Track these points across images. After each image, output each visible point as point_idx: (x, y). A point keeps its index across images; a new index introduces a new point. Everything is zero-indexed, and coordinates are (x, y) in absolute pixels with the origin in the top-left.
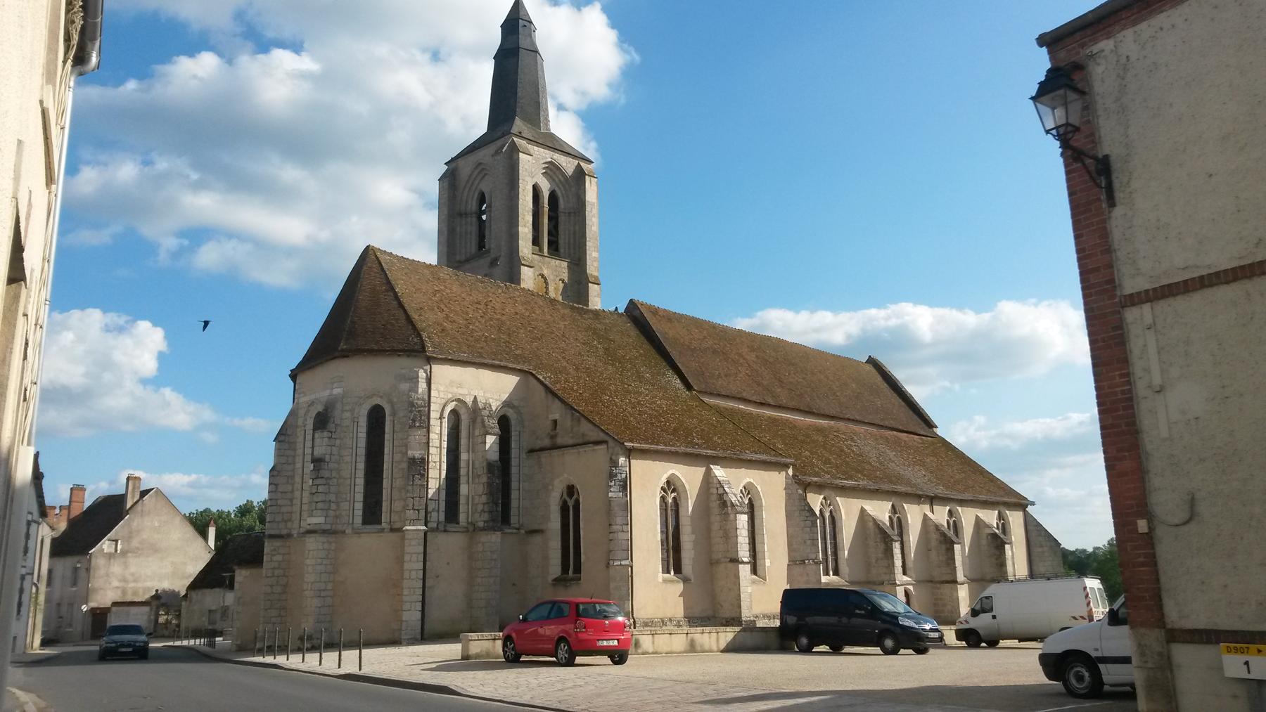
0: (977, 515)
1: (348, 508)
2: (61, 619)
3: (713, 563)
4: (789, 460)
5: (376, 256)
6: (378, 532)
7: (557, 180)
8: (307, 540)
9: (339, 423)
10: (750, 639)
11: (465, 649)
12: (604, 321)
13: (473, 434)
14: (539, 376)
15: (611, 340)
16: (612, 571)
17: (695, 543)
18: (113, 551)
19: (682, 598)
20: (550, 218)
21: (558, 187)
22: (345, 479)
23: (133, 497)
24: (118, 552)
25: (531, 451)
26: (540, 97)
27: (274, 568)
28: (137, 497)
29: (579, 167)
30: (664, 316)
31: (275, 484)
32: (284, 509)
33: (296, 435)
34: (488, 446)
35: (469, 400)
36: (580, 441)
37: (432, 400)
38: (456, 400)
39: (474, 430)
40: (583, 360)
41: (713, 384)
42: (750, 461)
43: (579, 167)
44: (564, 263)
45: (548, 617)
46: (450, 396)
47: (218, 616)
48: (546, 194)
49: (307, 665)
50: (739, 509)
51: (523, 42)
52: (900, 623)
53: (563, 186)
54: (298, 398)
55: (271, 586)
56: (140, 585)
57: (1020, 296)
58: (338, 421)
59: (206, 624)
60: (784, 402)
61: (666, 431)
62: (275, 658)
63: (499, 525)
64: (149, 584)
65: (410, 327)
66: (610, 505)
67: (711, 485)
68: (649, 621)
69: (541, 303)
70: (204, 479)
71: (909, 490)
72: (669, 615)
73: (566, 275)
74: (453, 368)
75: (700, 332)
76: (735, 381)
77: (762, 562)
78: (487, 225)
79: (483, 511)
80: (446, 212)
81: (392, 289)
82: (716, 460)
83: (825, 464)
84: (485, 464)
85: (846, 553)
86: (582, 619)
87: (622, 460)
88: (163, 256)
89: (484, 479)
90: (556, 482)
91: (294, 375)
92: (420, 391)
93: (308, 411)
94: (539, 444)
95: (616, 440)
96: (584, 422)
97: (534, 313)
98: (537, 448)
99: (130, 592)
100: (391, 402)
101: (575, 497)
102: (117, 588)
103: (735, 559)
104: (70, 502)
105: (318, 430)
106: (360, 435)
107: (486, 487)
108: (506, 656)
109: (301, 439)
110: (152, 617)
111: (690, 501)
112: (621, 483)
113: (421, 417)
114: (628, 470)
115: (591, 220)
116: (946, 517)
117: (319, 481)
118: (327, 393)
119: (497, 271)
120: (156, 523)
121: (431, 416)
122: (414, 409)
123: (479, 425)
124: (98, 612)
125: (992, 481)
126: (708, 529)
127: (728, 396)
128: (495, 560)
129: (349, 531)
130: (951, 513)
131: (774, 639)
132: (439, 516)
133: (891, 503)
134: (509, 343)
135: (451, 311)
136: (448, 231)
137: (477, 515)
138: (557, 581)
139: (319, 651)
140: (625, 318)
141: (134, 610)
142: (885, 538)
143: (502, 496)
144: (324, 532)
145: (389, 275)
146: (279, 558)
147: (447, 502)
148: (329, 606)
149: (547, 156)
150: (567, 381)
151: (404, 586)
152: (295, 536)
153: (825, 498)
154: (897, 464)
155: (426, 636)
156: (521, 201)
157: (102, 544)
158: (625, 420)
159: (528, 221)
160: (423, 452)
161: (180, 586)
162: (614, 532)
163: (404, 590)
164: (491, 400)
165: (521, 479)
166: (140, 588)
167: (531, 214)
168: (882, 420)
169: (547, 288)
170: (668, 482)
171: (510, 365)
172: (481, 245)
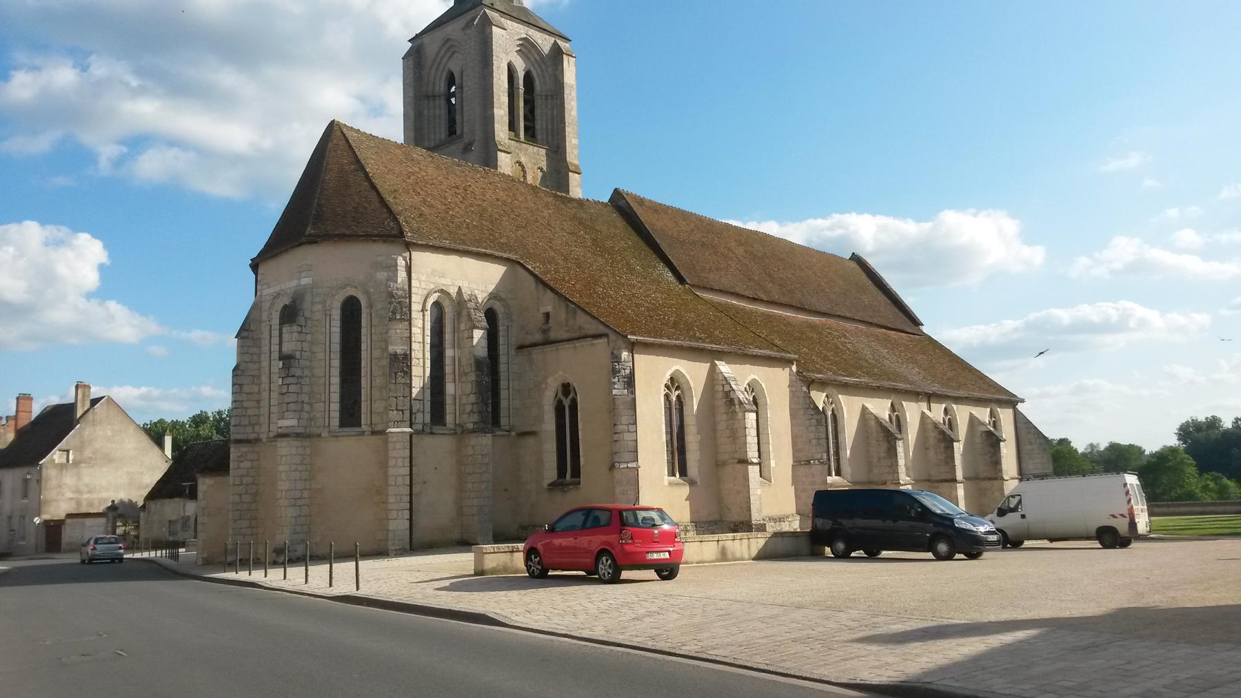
0: (971, 413)
1: (323, 409)
2: (12, 533)
3: (718, 464)
4: (793, 356)
5: (342, 132)
7: (532, 59)
9: (309, 316)
10: (782, 545)
11: (479, 561)
13: (459, 328)
14: (527, 266)
16: (617, 474)
17: (701, 443)
18: (65, 461)
19: (688, 502)
20: (526, 102)
21: (534, 66)
22: (320, 377)
23: (83, 405)
24: (70, 462)
25: (521, 347)
27: (242, 476)
28: (88, 405)
29: (556, 46)
30: (650, 207)
31: (239, 385)
32: (250, 412)
34: (475, 341)
36: (576, 335)
37: (413, 290)
40: (572, 251)
41: (706, 278)
43: (556, 46)
45: (584, 527)
46: (432, 286)
47: (179, 527)
48: (521, 75)
50: (748, 407)
52: (957, 525)
53: (539, 66)
54: (261, 290)
55: (240, 495)
56: (95, 496)
57: (960, 206)
58: (307, 314)
59: (167, 534)
60: (776, 297)
61: (667, 324)
62: (250, 574)
63: (490, 426)
64: (104, 495)
65: (385, 210)
66: (614, 403)
67: (716, 382)
70: (156, 392)
74: (434, 255)
75: (688, 224)
76: (726, 275)
77: (767, 462)
79: (472, 412)
80: (411, 94)
81: (362, 168)
82: (721, 355)
83: (824, 361)
85: (848, 452)
86: (626, 528)
87: (625, 355)
88: (104, 166)
90: (550, 380)
91: (255, 266)
92: (399, 280)
93: (273, 304)
94: (530, 339)
95: (618, 333)
96: (580, 313)
98: (528, 343)
99: (84, 503)
100: (367, 293)
102: (71, 499)
104: (17, 411)
105: (286, 324)
106: (333, 329)
107: (474, 385)
108: (531, 571)
109: (266, 335)
111: (694, 399)
112: (626, 380)
114: (631, 365)
115: (570, 103)
116: (942, 415)
117: (290, 380)
118: (294, 283)
120: (109, 432)
121: (413, 309)
122: (393, 300)
123: (464, 318)
124: (52, 524)
125: (981, 379)
126: (714, 429)
128: (486, 464)
129: (325, 434)
130: (946, 411)
131: (804, 544)
133: (891, 401)
135: (428, 195)
137: (465, 416)
138: (553, 486)
139: (304, 563)
140: (610, 209)
141: (89, 521)
142: (888, 437)
143: (492, 395)
144: (298, 435)
145: (358, 154)
146: (247, 464)
147: (433, 403)
148: (306, 516)
149: (522, 31)
150: (557, 271)
152: (264, 440)
153: (827, 396)
154: (891, 361)
155: (417, 546)
157: (52, 455)
158: (623, 313)
159: (504, 103)
160: (406, 347)
161: (138, 497)
164: (477, 292)
165: (510, 378)
166: (94, 499)
167: (506, 94)
168: (871, 317)
170: (672, 379)
171: (497, 254)
172: (452, 131)
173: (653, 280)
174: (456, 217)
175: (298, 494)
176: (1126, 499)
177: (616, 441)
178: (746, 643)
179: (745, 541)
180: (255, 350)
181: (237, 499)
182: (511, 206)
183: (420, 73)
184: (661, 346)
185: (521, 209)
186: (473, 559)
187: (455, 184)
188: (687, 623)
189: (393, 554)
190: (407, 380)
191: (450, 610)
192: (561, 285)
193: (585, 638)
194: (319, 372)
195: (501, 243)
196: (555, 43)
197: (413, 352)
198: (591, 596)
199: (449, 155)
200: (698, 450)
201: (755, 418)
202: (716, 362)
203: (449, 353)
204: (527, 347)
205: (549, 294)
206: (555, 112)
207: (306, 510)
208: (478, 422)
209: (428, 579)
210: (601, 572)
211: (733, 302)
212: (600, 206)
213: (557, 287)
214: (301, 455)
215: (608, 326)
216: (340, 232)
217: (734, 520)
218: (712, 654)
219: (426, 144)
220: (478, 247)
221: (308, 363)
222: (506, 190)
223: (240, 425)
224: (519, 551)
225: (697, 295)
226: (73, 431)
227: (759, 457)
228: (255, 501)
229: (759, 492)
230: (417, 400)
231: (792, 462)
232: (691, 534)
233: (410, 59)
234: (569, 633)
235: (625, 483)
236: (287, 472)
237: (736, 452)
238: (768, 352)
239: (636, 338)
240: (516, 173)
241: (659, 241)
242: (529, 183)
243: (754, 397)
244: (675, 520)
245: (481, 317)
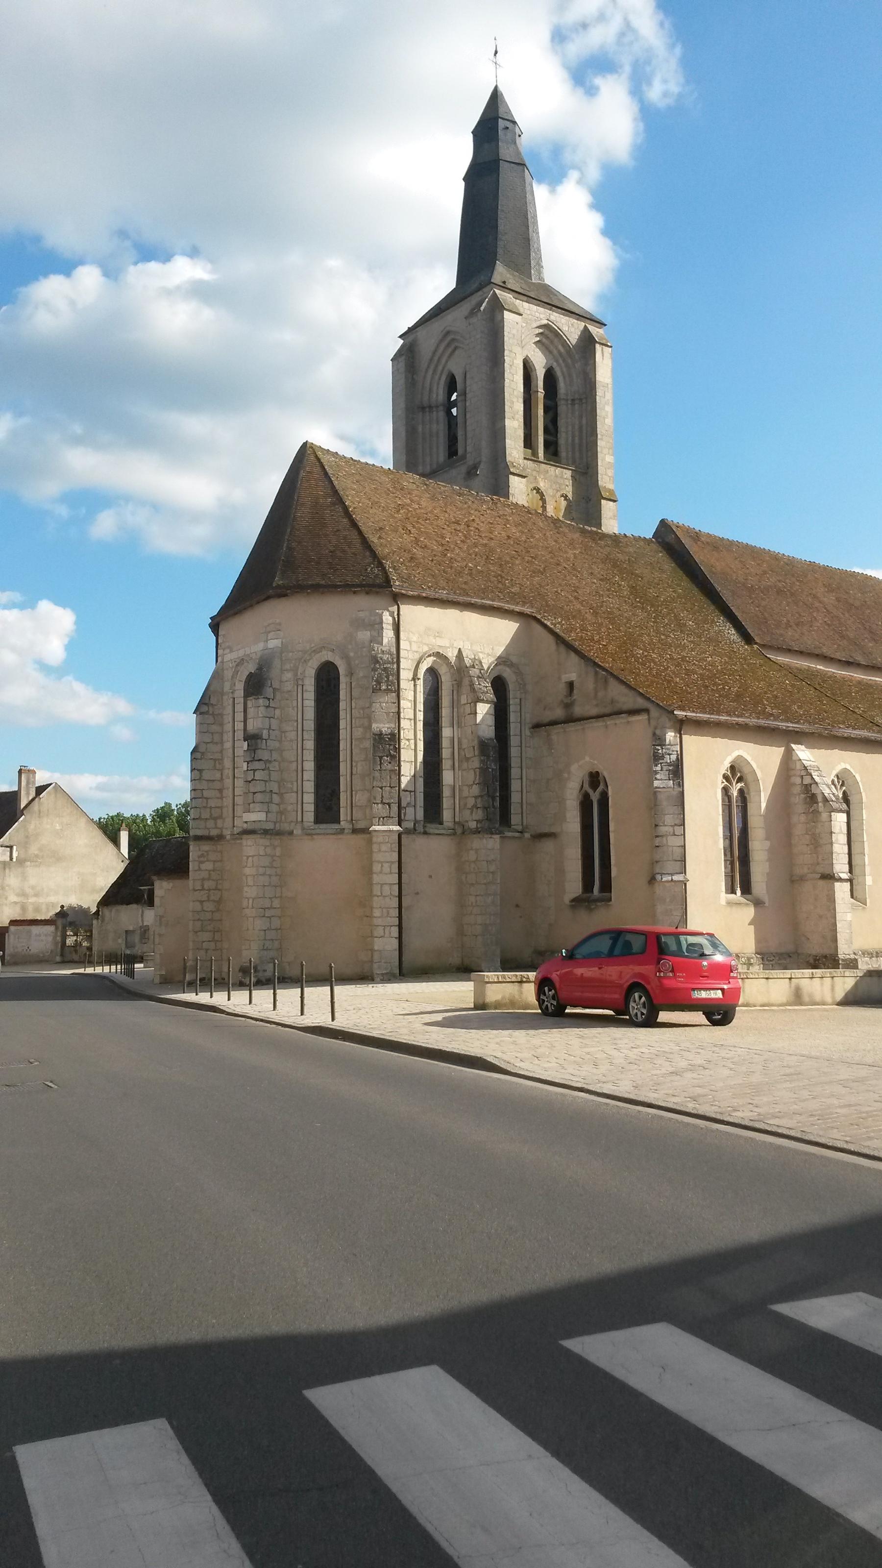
5: (316, 457)
7: (555, 352)
8: (244, 842)
9: (278, 687)
11: (479, 992)
12: (627, 550)
13: (459, 701)
14: (545, 622)
15: (637, 576)
16: (658, 890)
17: (771, 851)
20: (546, 410)
21: (557, 361)
22: (291, 762)
23: (28, 794)
24: (14, 860)
25: (537, 726)
26: (530, 230)
27: (203, 879)
28: (33, 794)
30: (708, 543)
32: (212, 803)
33: (222, 705)
34: (479, 718)
36: (607, 710)
38: (433, 655)
39: (459, 696)
41: (781, 635)
43: (586, 332)
46: (426, 649)
47: (137, 938)
49: (255, 1008)
50: (835, 805)
51: (505, 152)
53: (564, 361)
56: (41, 900)
58: (276, 685)
59: (123, 947)
61: (727, 696)
62: (211, 997)
63: (497, 825)
64: (52, 899)
65: (368, 553)
66: (656, 798)
67: (792, 773)
69: (541, 524)
75: (758, 564)
76: (809, 631)
77: (860, 879)
78: (460, 421)
80: (403, 405)
81: (341, 502)
82: (799, 737)
84: (476, 743)
86: (667, 957)
87: (670, 736)
89: (476, 763)
90: (574, 768)
91: (215, 625)
92: (385, 641)
94: (549, 716)
96: (612, 682)
97: (532, 537)
98: (546, 720)
101: (601, 787)
102: (16, 903)
103: (829, 874)
106: (306, 703)
108: (544, 1007)
109: (229, 709)
110: (59, 939)
112: (671, 768)
113: (388, 677)
114: (679, 750)
117: (256, 765)
118: (261, 646)
119: (476, 482)
121: (402, 677)
123: (465, 689)
126: (788, 833)
127: (801, 653)
129: (297, 831)
132: (416, 812)
134: (502, 577)
136: (407, 431)
137: (468, 812)
138: (577, 902)
140: (655, 546)
141: (35, 930)
144: (266, 832)
145: (336, 483)
146: (209, 866)
147: (426, 795)
149: (542, 316)
151: (375, 905)
152: (228, 837)
158: (669, 682)
161: (90, 901)
163: (375, 910)
164: (481, 656)
165: (524, 764)
167: (521, 400)
170: (732, 768)
171: (507, 606)
172: (452, 451)
173: (710, 640)
174: (455, 560)
177: (658, 846)
178: (820, 1112)
179: (828, 981)
180: (215, 728)
181: (198, 907)
182: (526, 546)
183: (413, 379)
184: (718, 725)
185: (538, 549)
186: (473, 989)
187: (454, 517)
188: (741, 1082)
189: (379, 979)
190: (394, 766)
191: (440, 1050)
192: (589, 646)
193: (606, 1094)
194: (290, 755)
195: (512, 593)
196: (585, 326)
197: (402, 732)
198: (619, 1042)
199: (450, 482)
200: (767, 861)
201: (846, 820)
202: (792, 745)
203: (446, 732)
204: (545, 725)
205: (574, 657)
206: (584, 421)
207: (276, 923)
208: (482, 820)
209: (418, 1011)
210: (633, 1012)
211: (818, 667)
212: (642, 543)
213: (583, 648)
215: (648, 699)
216: (314, 583)
217: (814, 953)
218: (772, 1124)
219: (420, 469)
220: (483, 599)
221: (277, 744)
222: (520, 524)
223: (199, 819)
224: (530, 982)
225: (769, 658)
226: (16, 824)
227: (851, 871)
228: (218, 910)
229: (849, 917)
230: (407, 791)
232: (757, 969)
233: (400, 360)
234: (586, 1086)
236: (254, 876)
238: (864, 733)
239: (685, 714)
240: (533, 503)
241: (719, 589)
242: (549, 515)
243: (844, 793)
244: (733, 949)
245: (486, 687)
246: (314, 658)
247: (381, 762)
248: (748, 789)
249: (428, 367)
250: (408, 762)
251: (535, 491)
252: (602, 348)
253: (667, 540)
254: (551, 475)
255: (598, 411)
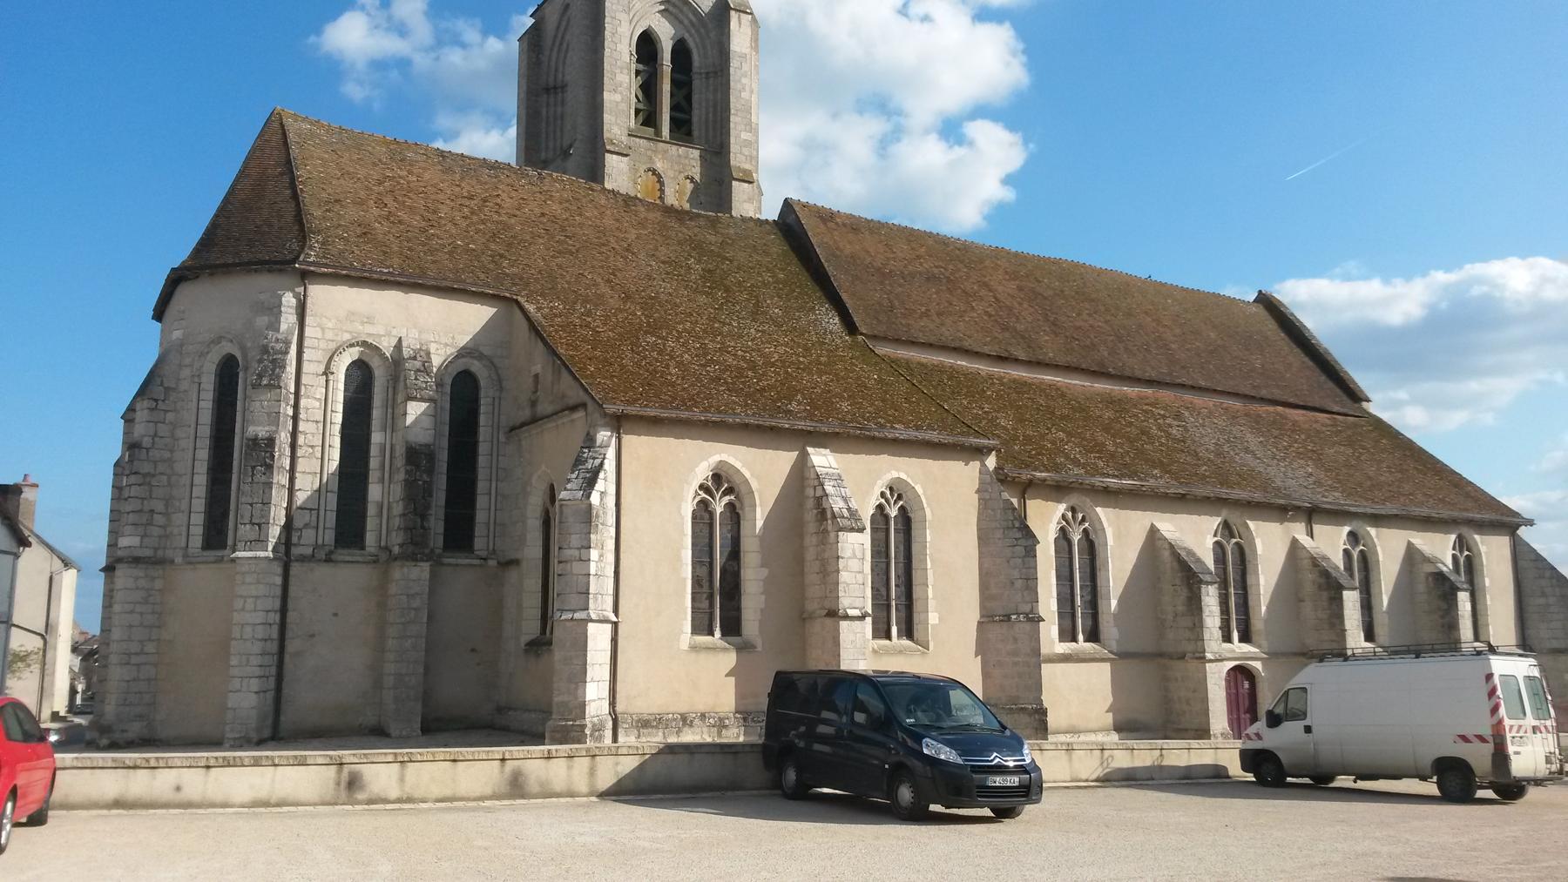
0: (1152, 524)
3: (804, 618)
5: (281, 124)
6: (215, 562)
7: (686, 22)
17: (768, 583)
20: (675, 83)
21: (688, 31)
35: (387, 346)
42: (895, 441)
44: (694, 151)
46: (347, 337)
53: (697, 31)
60: (1050, 355)
68: (652, 718)
71: (1258, 496)
72: (701, 708)
73: (698, 169)
77: (922, 616)
80: (525, 88)
87: (603, 435)
92: (283, 327)
111: (758, 510)
113: (273, 370)
115: (740, 81)
125: (1456, 486)
127: (931, 345)
129: (179, 560)
130: (1354, 537)
131: (753, 769)
142: (1188, 578)
147: (340, 512)
156: (607, 52)
162: (566, 562)
163: (232, 657)
169: (662, 191)
170: (717, 478)
175: (135, 647)
176: (1487, 706)
189: (227, 745)
214: (143, 588)
221: (167, 455)
231: (979, 617)
235: (568, 644)
237: (826, 597)
246: (213, 350)
247: (253, 471)
248: (742, 504)
249: (553, 44)
250: (309, 473)
251: (650, 173)
252: (739, 16)
253: (788, 221)
254: (672, 155)
255: (732, 84)
